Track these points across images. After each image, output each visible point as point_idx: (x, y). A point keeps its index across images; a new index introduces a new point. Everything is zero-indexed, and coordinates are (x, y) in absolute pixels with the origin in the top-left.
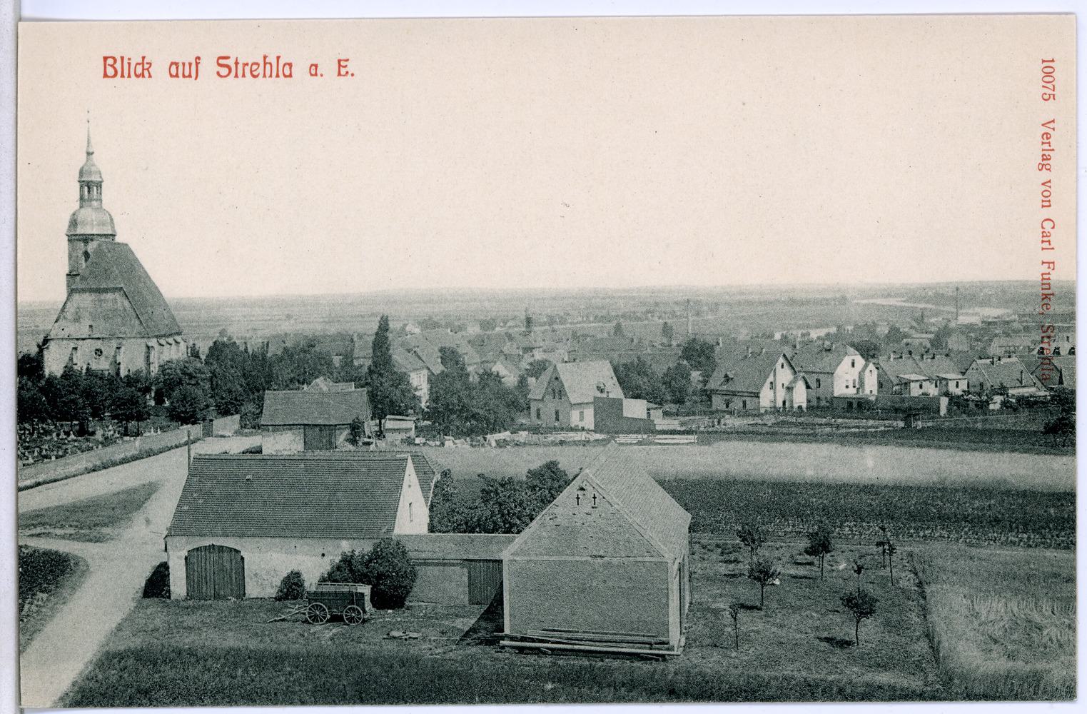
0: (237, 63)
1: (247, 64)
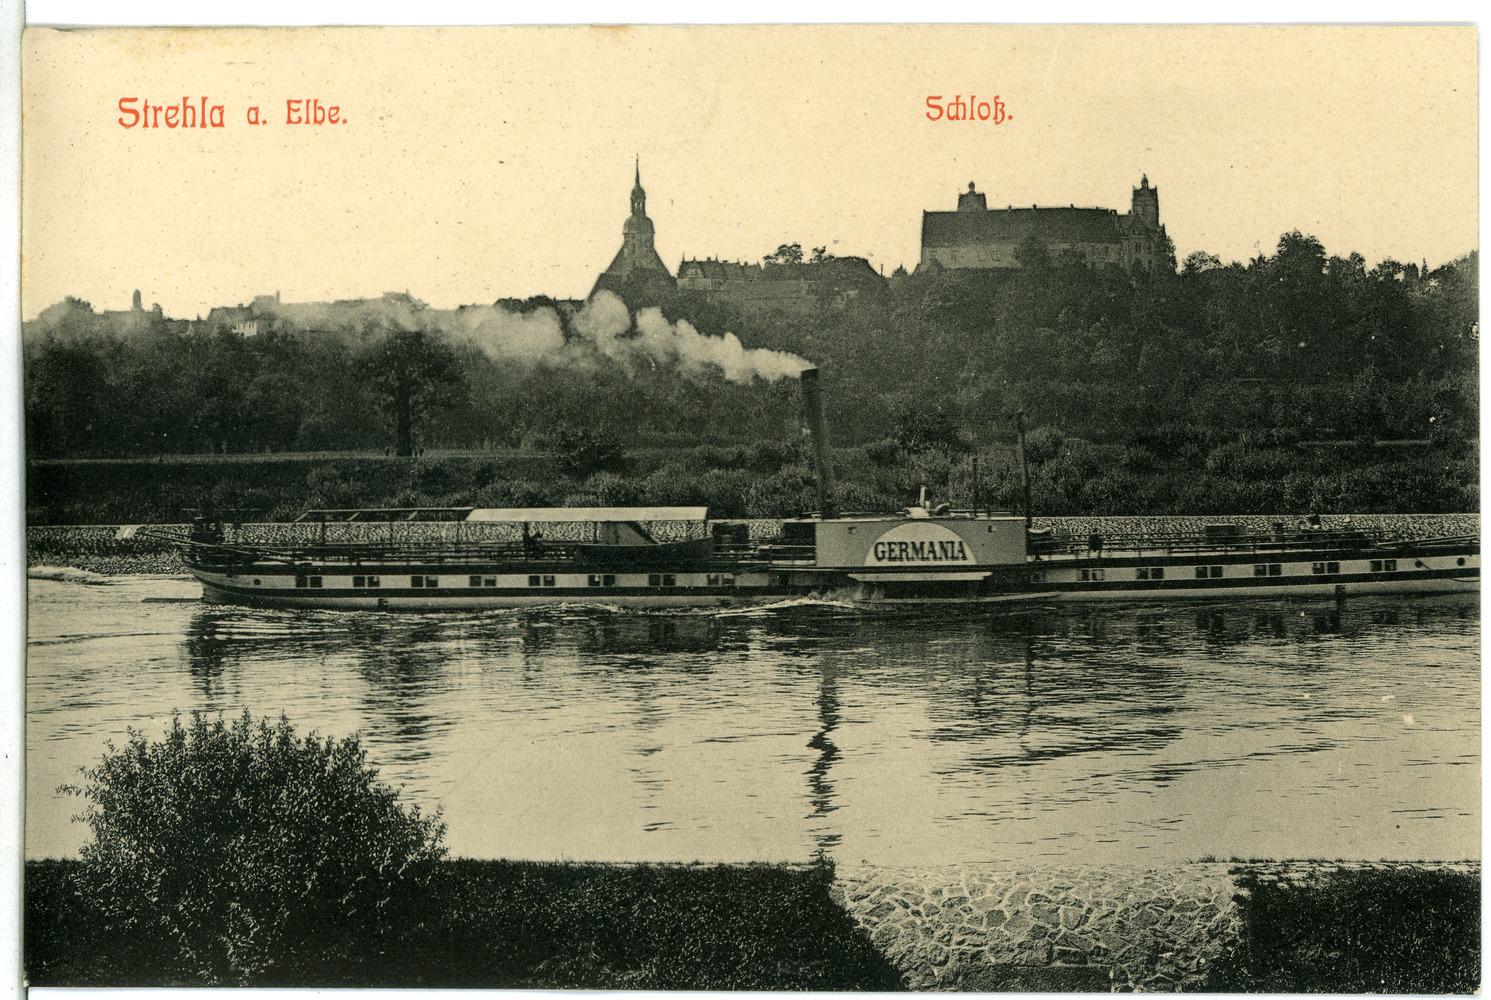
0: (146, 108)
1: (161, 108)
